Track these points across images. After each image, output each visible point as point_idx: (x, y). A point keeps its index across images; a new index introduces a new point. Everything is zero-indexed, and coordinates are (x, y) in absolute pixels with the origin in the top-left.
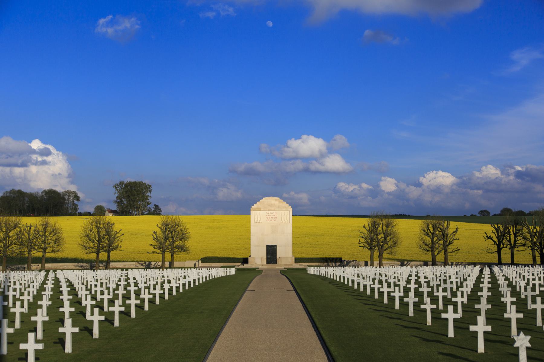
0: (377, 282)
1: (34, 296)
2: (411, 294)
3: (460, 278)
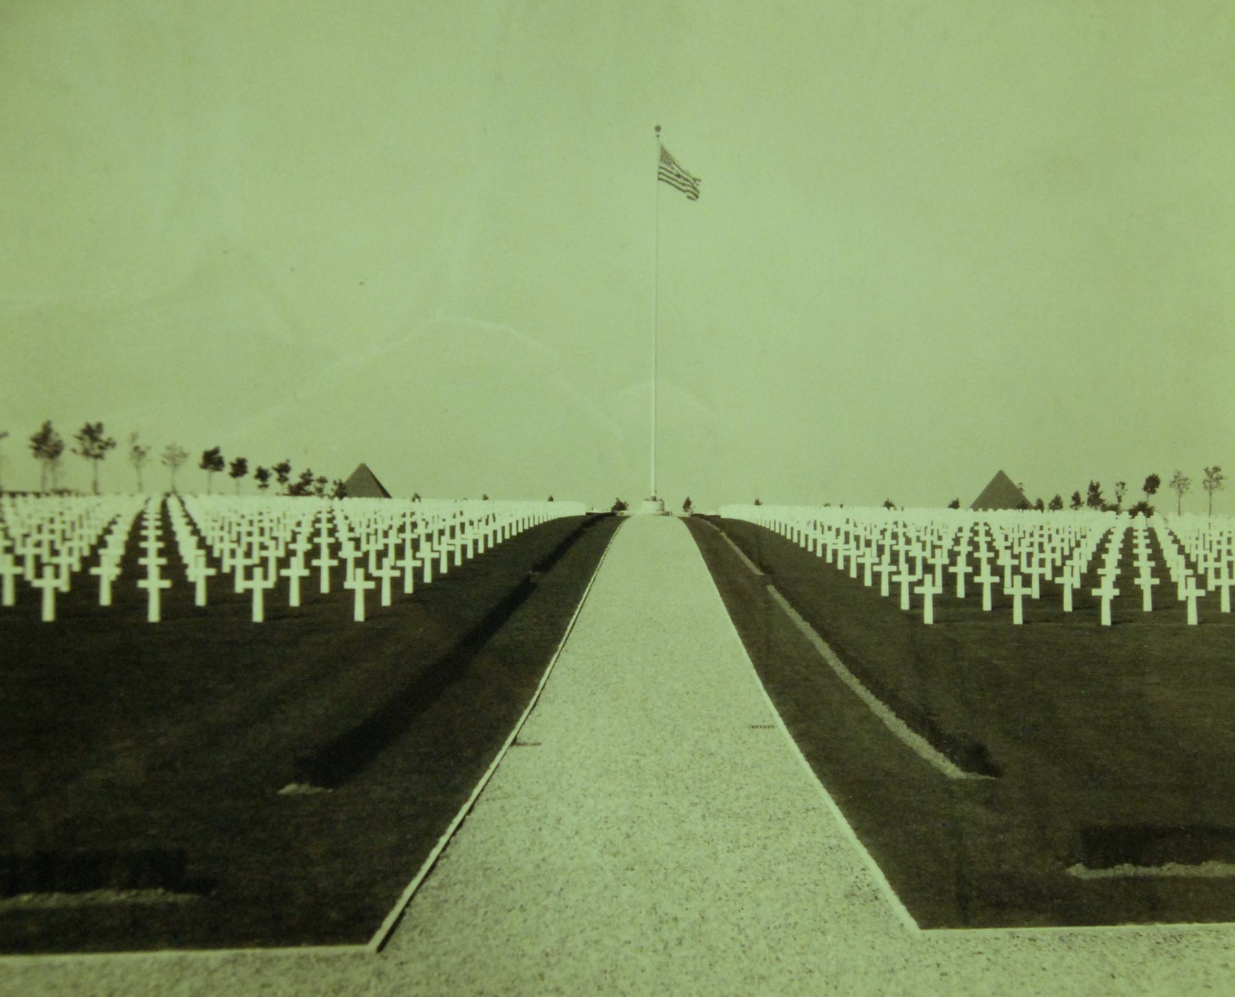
0: (888, 535)
1: (1083, 576)
2: (962, 560)
3: (1076, 533)
